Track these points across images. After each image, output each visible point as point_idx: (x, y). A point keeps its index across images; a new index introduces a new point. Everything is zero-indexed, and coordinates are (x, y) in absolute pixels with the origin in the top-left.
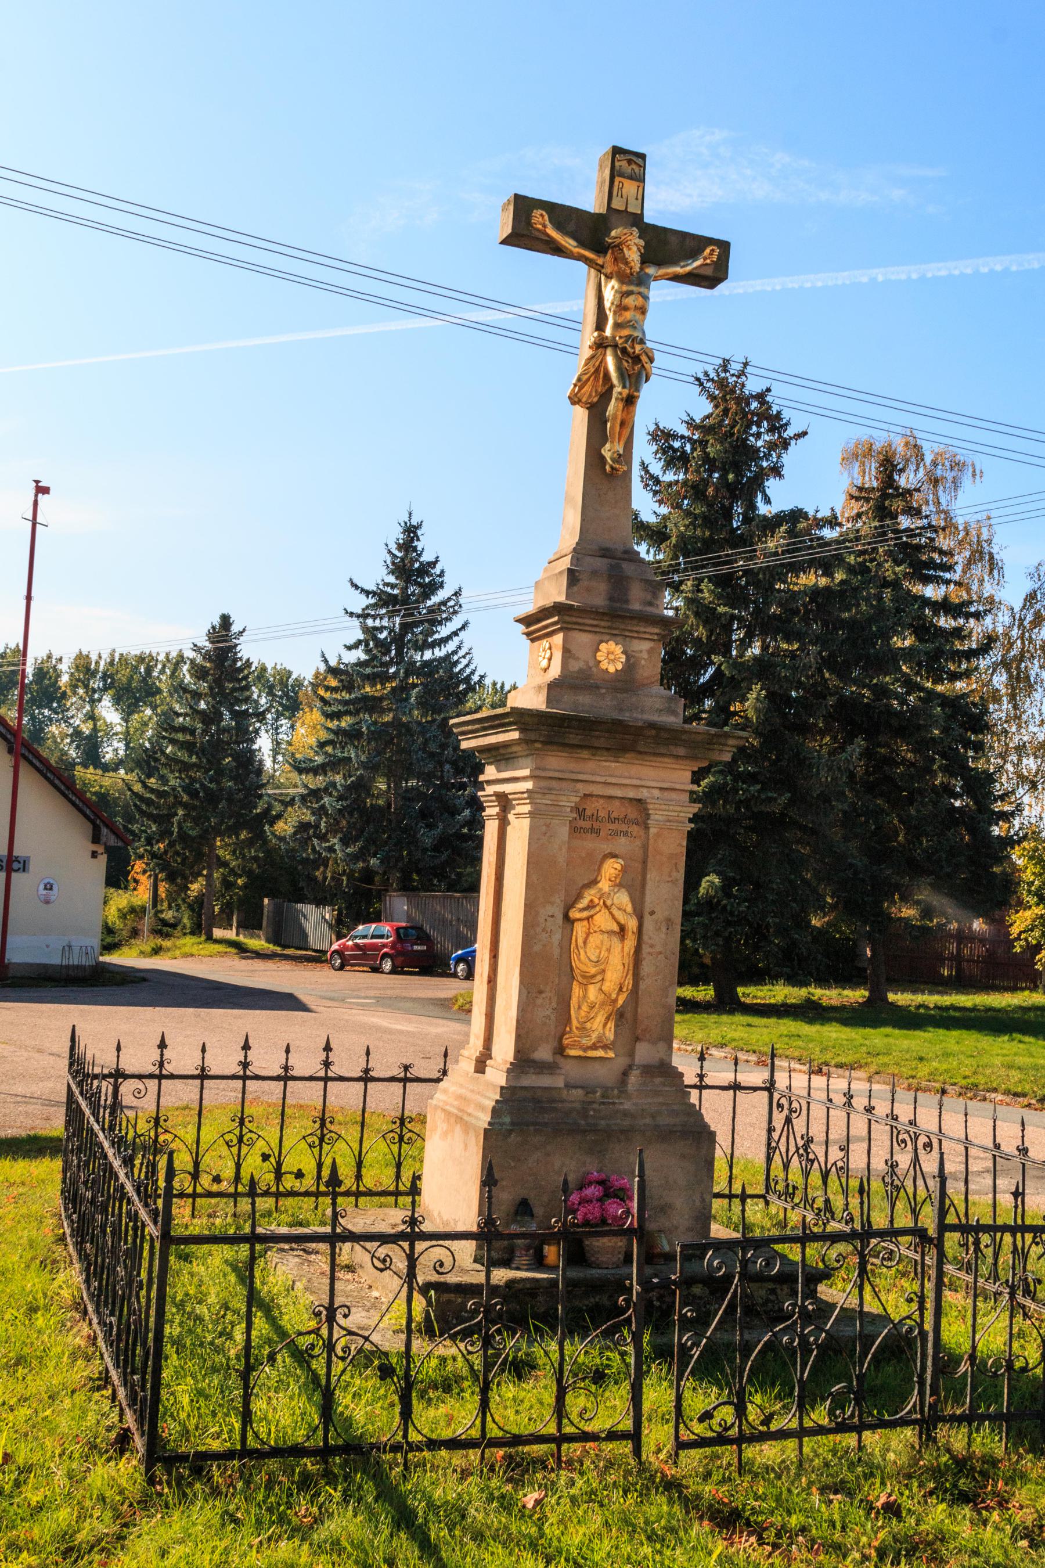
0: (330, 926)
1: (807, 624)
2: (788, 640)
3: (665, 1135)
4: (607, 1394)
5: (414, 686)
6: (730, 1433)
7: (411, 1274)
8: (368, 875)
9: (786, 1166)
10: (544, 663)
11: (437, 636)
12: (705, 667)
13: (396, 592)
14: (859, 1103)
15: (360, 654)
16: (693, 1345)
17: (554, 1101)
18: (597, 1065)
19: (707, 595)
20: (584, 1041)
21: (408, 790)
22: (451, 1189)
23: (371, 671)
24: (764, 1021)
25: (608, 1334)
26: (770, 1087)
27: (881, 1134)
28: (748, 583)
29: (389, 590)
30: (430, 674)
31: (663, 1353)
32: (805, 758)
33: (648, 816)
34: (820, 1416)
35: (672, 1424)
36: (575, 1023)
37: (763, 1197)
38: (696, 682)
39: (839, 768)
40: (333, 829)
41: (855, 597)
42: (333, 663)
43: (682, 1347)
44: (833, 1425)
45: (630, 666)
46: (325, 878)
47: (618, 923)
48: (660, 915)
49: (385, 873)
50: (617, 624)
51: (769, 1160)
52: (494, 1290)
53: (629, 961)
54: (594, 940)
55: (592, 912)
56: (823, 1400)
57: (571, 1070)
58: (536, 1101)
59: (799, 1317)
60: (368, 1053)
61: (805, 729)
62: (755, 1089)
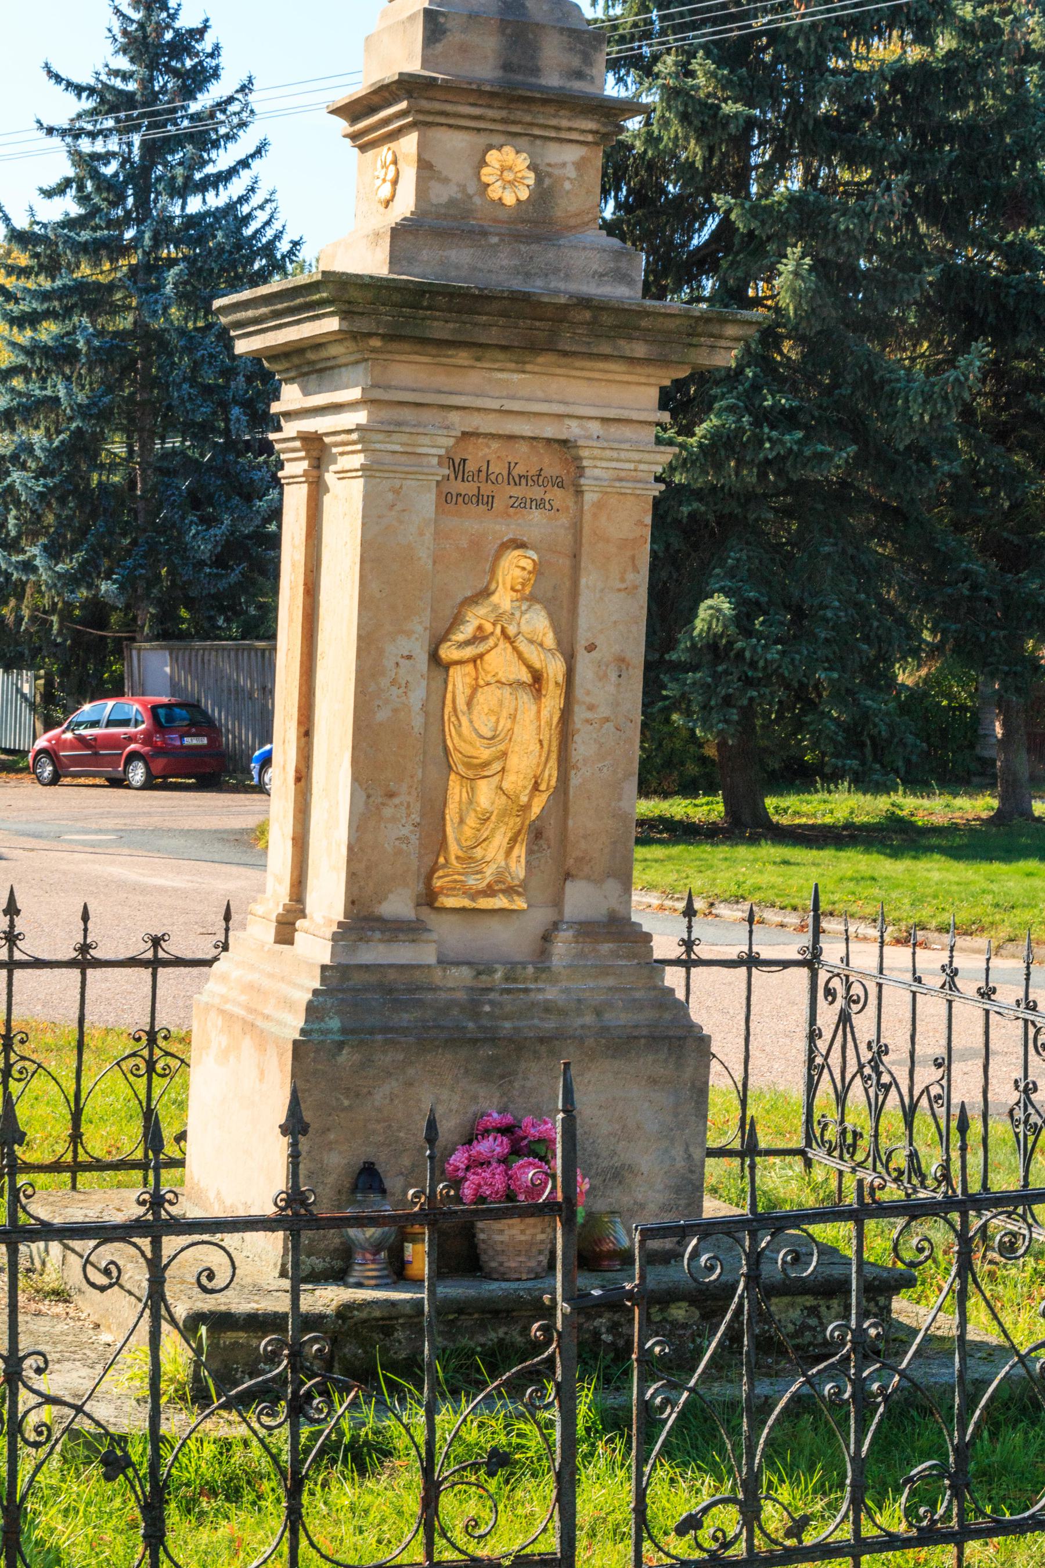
0: (33, 707)
1: (887, 134)
2: (851, 161)
3: (620, 1045)
4: (519, 1494)
5: (172, 262)
6: (730, 1552)
7: (156, 1297)
8: (97, 613)
9: (841, 1099)
10: (386, 191)
11: (210, 169)
12: (701, 216)
13: (132, 86)
14: (968, 985)
15: (68, 206)
16: (666, 1402)
17: (419, 989)
18: (495, 924)
19: (701, 80)
20: (472, 881)
21: (167, 455)
22: (236, 1148)
23: (90, 236)
24: (813, 854)
25: (515, 1388)
26: (812, 961)
27: (1007, 1034)
28: (776, 59)
29: (118, 83)
30: (200, 241)
31: (613, 1421)
32: (883, 382)
33: (580, 470)
34: (892, 1518)
35: (630, 1542)
36: (453, 848)
37: (801, 1152)
38: (686, 244)
39: (945, 399)
40: (32, 529)
41: (973, 82)
42: (21, 223)
43: (646, 1406)
44: (914, 1532)
45: (544, 193)
46: (19, 620)
47: (529, 667)
48: (606, 651)
49: (128, 607)
50: (518, 115)
51: (811, 1087)
52: (310, 1322)
53: (550, 736)
54: (487, 698)
55: (481, 648)
56: (898, 1490)
57: (447, 933)
58: (388, 990)
59: (853, 1349)
60: (85, 917)
61: (884, 330)
62: (785, 964)
